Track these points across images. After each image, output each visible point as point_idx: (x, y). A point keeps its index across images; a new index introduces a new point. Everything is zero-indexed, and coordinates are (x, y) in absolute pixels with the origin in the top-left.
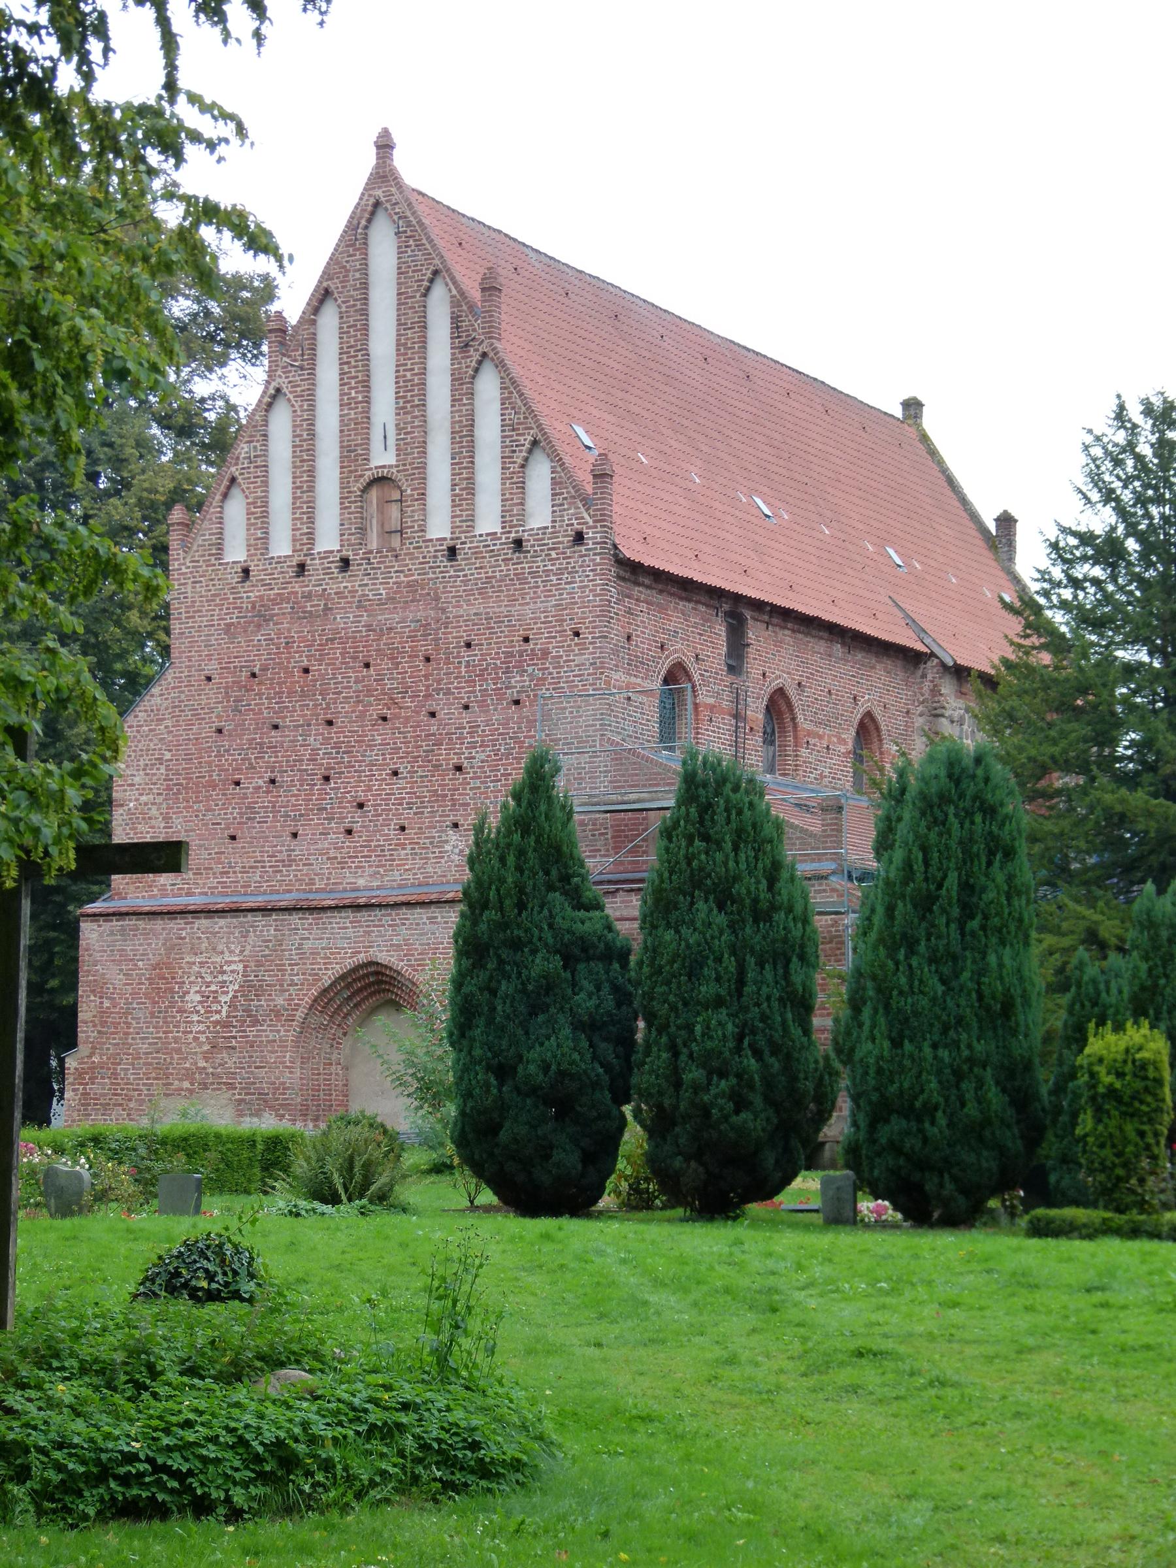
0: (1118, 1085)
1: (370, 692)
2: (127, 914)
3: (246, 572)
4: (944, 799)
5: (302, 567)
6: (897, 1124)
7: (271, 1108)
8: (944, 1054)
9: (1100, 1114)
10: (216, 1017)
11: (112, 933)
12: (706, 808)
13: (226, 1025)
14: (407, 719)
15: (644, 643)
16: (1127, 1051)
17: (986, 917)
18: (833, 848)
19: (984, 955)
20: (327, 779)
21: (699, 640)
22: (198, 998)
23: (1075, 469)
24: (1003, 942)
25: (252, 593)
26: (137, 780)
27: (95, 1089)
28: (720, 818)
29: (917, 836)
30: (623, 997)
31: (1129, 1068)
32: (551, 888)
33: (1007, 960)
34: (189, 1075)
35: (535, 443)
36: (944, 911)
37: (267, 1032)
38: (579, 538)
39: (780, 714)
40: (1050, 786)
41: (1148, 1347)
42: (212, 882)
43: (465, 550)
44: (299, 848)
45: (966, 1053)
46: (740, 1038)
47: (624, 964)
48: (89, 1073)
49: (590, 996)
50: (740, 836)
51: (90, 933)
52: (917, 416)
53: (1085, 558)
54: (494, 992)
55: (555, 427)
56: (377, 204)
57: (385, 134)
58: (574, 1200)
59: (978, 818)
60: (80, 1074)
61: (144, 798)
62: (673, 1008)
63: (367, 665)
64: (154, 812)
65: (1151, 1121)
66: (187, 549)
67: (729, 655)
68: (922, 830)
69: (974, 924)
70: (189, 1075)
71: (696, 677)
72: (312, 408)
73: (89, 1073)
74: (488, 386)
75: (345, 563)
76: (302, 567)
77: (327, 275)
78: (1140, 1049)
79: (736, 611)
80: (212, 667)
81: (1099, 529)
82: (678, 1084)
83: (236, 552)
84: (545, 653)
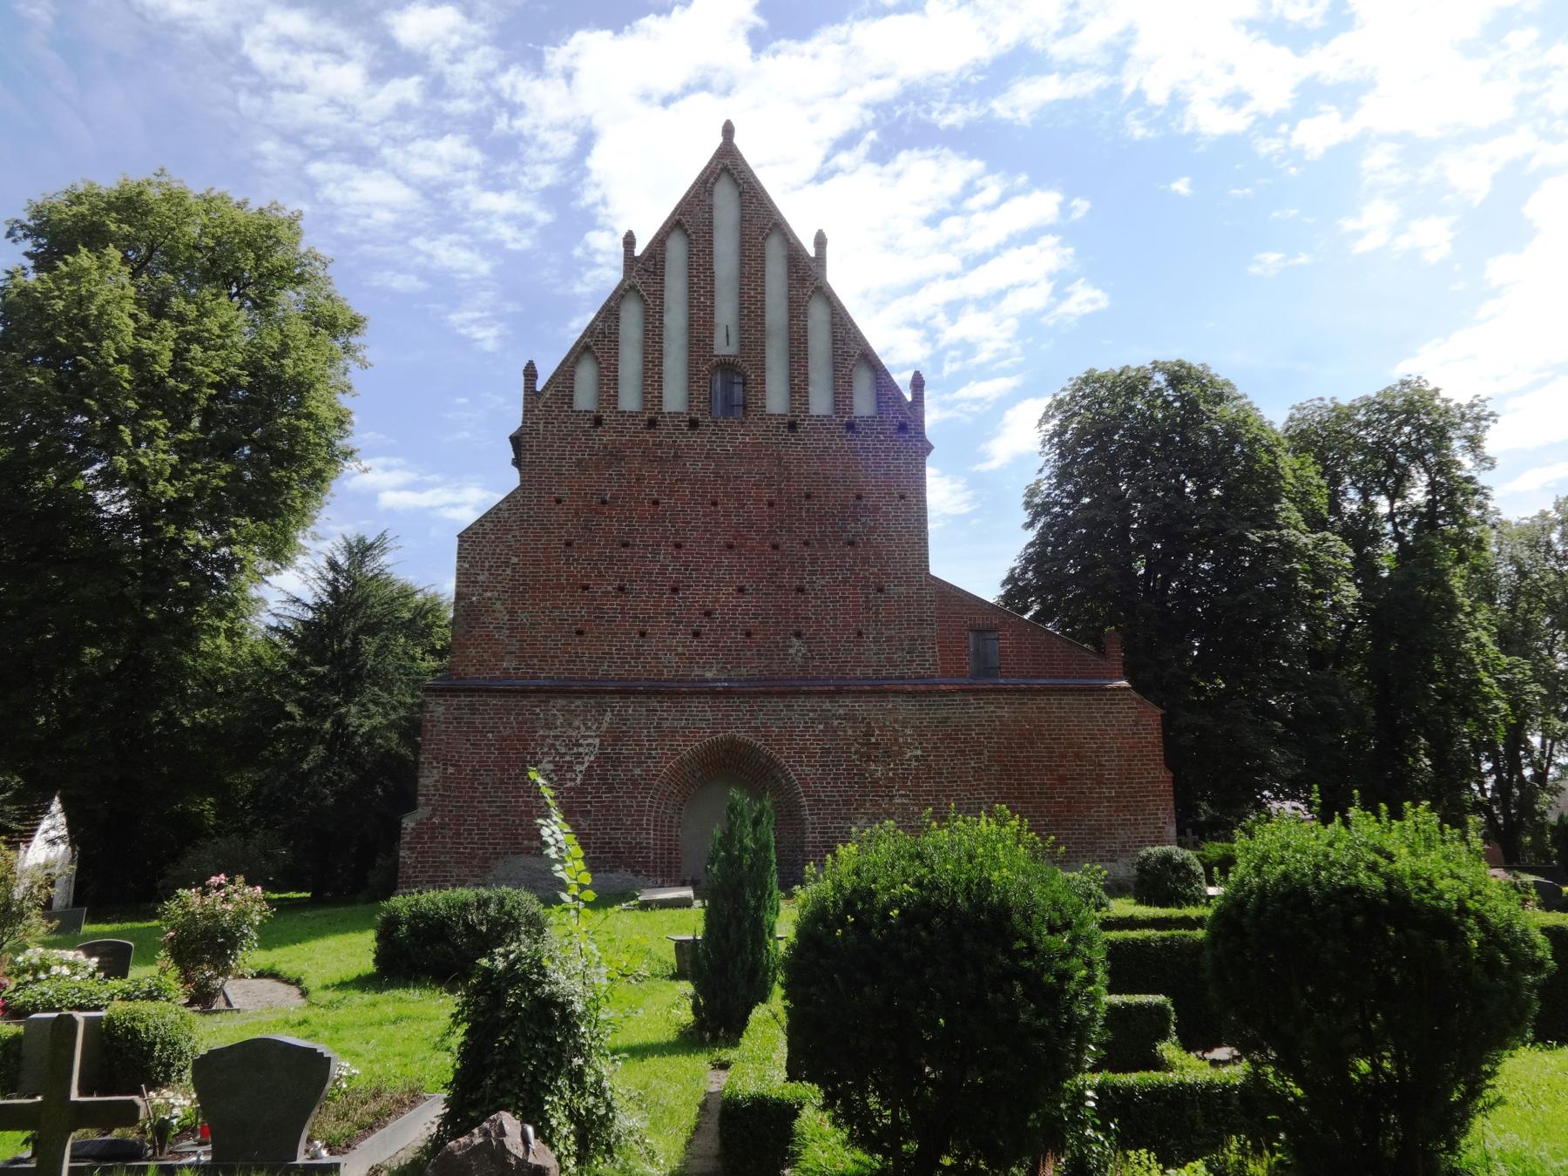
2: (477, 690)
7: (628, 865)
10: (570, 784)
11: (459, 708)
14: (753, 549)
20: (675, 590)
22: (551, 767)
26: (481, 578)
40: (486, 230)
61: (489, 594)
63: (715, 504)
64: (498, 605)
84: (876, 509)
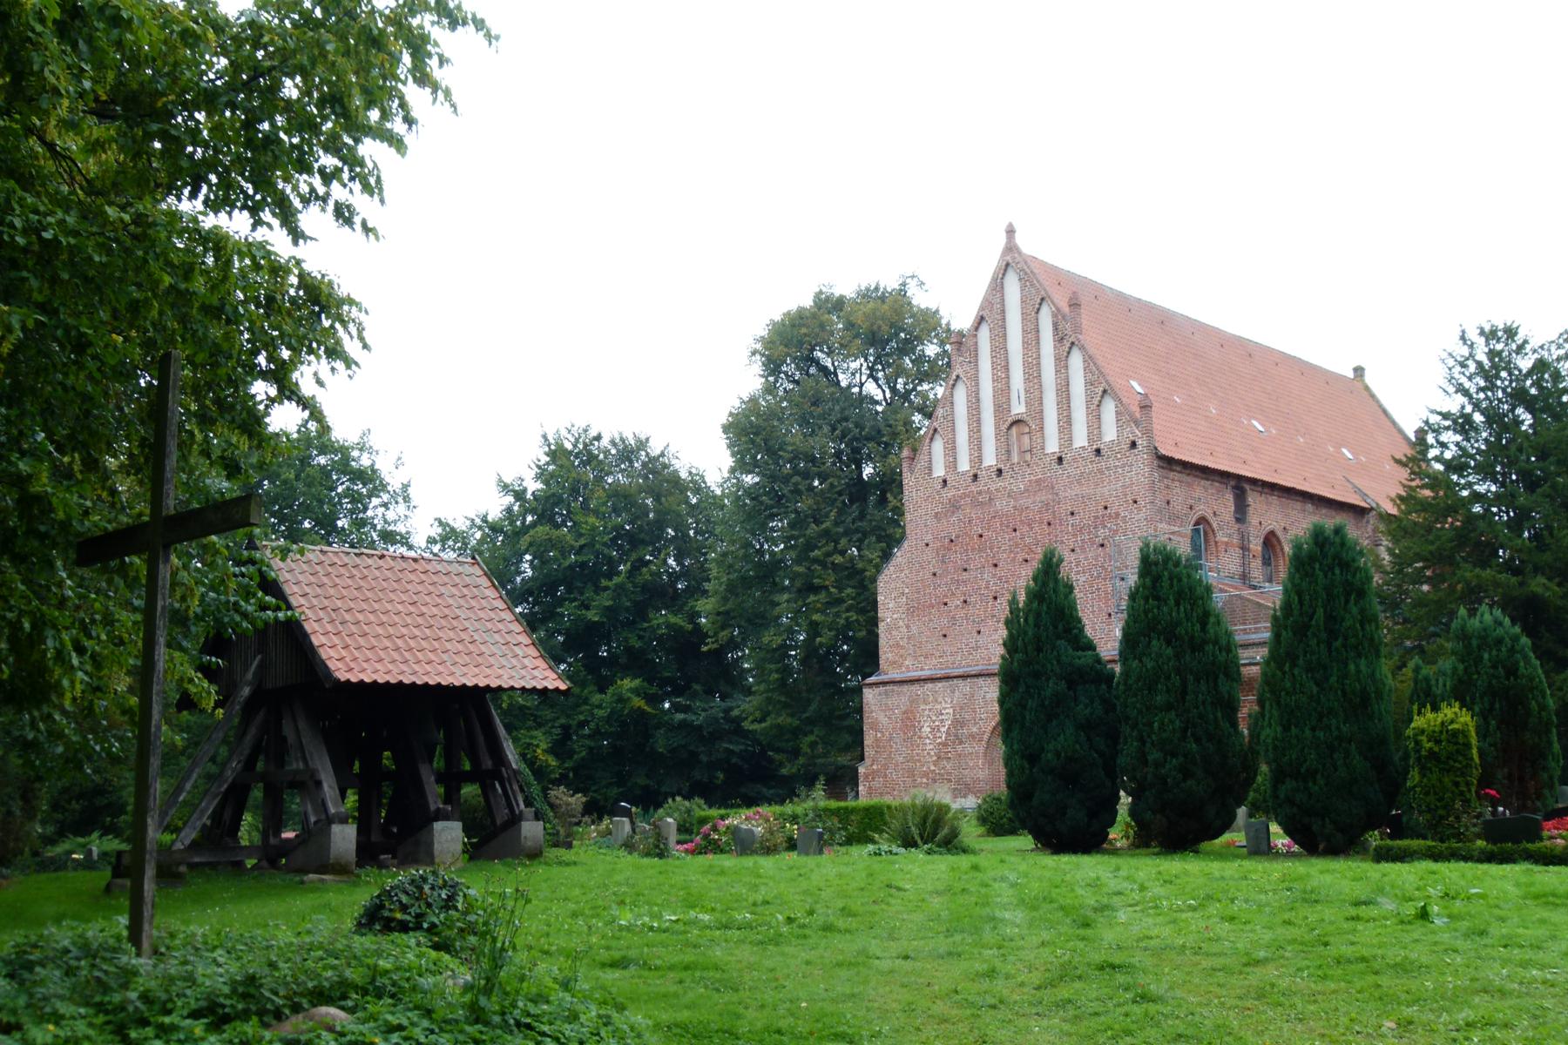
0: (1436, 749)
1: (1017, 545)
3: (945, 481)
4: (1312, 558)
5: (975, 476)
6: (1290, 784)
8: (1321, 734)
9: (1424, 771)
12: (1157, 579)
13: (945, 744)
15: (1178, 505)
16: (1442, 723)
17: (1346, 639)
18: (1247, 598)
19: (1346, 665)
21: (1218, 505)
23: (1439, 375)
24: (1359, 656)
25: (949, 494)
27: (875, 784)
28: (1166, 584)
29: (1294, 585)
30: (1109, 706)
31: (1444, 736)
32: (1059, 638)
33: (1363, 668)
34: (926, 775)
35: (1105, 391)
36: (1314, 635)
37: (968, 748)
38: (1133, 445)
39: (1273, 547)
41: (1363, 959)
42: (935, 661)
43: (1067, 457)
44: (982, 640)
45: (1336, 733)
46: (1185, 730)
47: (1110, 687)
48: (872, 775)
49: (1086, 706)
50: (1180, 597)
51: (868, 694)
52: (1362, 376)
53: (1447, 428)
54: (1024, 707)
55: (1117, 382)
56: (1007, 265)
57: (1011, 225)
58: (1088, 840)
59: (1337, 571)
60: (866, 776)
62: (1140, 712)
65: (1463, 775)
66: (912, 472)
67: (1236, 511)
68: (1297, 581)
69: (1338, 643)
70: (926, 775)
71: (1215, 525)
72: (977, 384)
73: (872, 775)
74: (1076, 360)
75: (1000, 472)
76: (975, 476)
77: (982, 308)
78: (1452, 722)
79: (1240, 485)
80: (928, 538)
81: (1455, 409)
82: (1146, 763)
83: (939, 471)
84: (1117, 515)
